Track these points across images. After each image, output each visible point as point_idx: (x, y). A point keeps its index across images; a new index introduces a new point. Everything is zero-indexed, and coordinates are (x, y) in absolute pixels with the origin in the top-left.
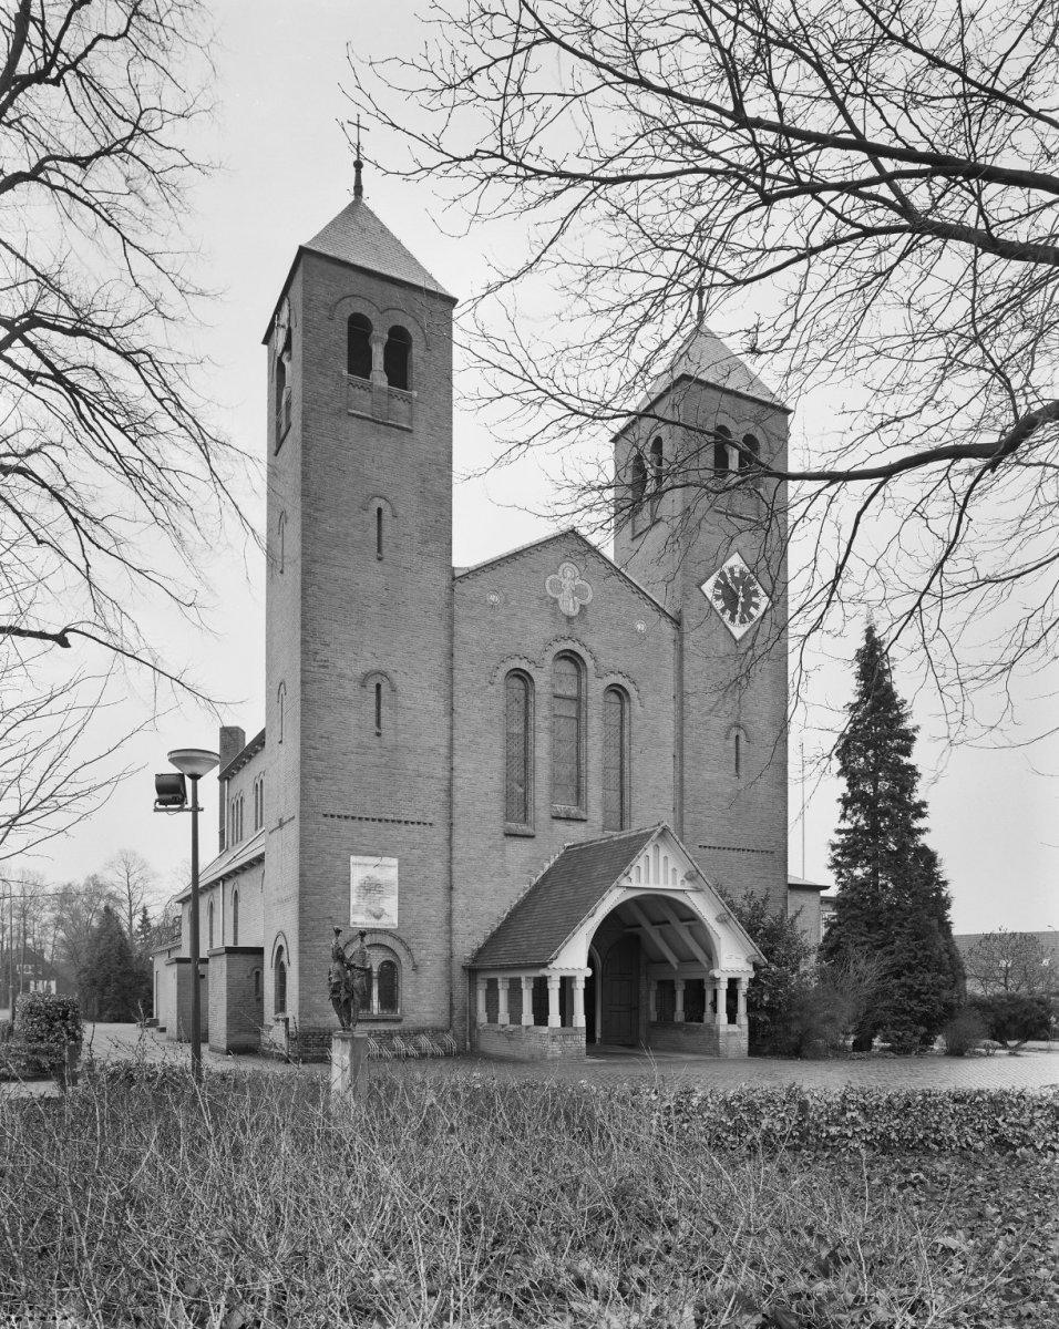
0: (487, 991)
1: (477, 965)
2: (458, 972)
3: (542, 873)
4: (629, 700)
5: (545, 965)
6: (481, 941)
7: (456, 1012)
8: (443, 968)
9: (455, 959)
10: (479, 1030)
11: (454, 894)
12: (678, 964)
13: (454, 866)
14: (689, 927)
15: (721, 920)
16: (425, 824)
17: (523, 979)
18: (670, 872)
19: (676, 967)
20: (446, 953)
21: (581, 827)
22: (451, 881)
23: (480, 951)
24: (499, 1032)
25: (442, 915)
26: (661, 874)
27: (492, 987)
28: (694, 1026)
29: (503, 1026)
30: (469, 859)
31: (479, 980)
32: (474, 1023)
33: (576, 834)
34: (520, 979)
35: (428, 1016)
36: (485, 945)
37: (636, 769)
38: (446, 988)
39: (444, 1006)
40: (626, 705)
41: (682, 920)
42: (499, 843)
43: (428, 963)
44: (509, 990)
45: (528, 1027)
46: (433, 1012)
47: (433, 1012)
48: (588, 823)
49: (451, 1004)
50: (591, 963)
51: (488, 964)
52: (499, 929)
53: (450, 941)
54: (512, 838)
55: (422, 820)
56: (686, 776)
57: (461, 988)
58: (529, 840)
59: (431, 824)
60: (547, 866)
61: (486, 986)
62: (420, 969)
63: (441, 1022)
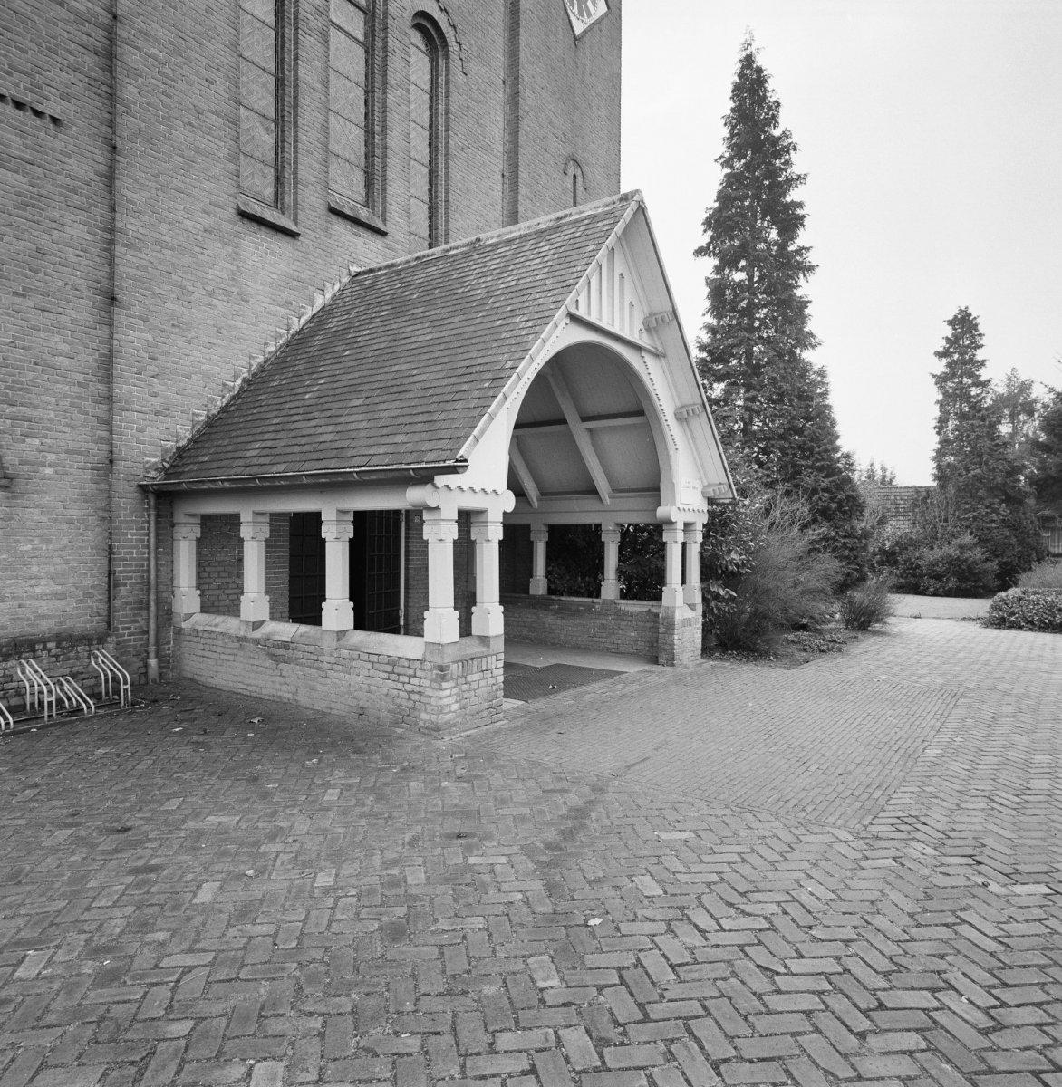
0: (200, 542)
1: (184, 482)
2: (126, 498)
3: (310, 312)
4: (447, 56)
5: (424, 477)
6: (185, 432)
7: (123, 591)
8: (91, 488)
9: (120, 466)
10: (179, 631)
11: (120, 316)
12: (539, 500)
13: (119, 250)
14: (590, 430)
15: (683, 417)
16: (38, 114)
17: (246, 517)
18: (627, 306)
19: (536, 504)
20: (100, 451)
21: (375, 243)
22: (111, 277)
23: (181, 453)
24: (242, 640)
25: (89, 358)
26: (617, 301)
27: (219, 534)
28: (581, 604)
29: (257, 625)
30: (158, 242)
31: (180, 517)
32: (166, 615)
33: (368, 253)
34: (237, 516)
35: (44, 607)
36: (194, 440)
37: (456, 175)
38: (93, 537)
39: (93, 579)
40: (442, 62)
41: (584, 419)
42: (227, 227)
43: (49, 471)
44: (198, 540)
45: (341, 634)
46: (60, 596)
47: (60, 596)
48: (388, 240)
49: (110, 574)
50: (514, 485)
51: (221, 477)
52: (224, 410)
53: (108, 422)
54: (256, 227)
55: (27, 98)
56: (521, 209)
57: (134, 536)
58: (288, 239)
59: (55, 120)
60: (320, 301)
61: (197, 532)
62: (20, 485)
63: (82, 619)
